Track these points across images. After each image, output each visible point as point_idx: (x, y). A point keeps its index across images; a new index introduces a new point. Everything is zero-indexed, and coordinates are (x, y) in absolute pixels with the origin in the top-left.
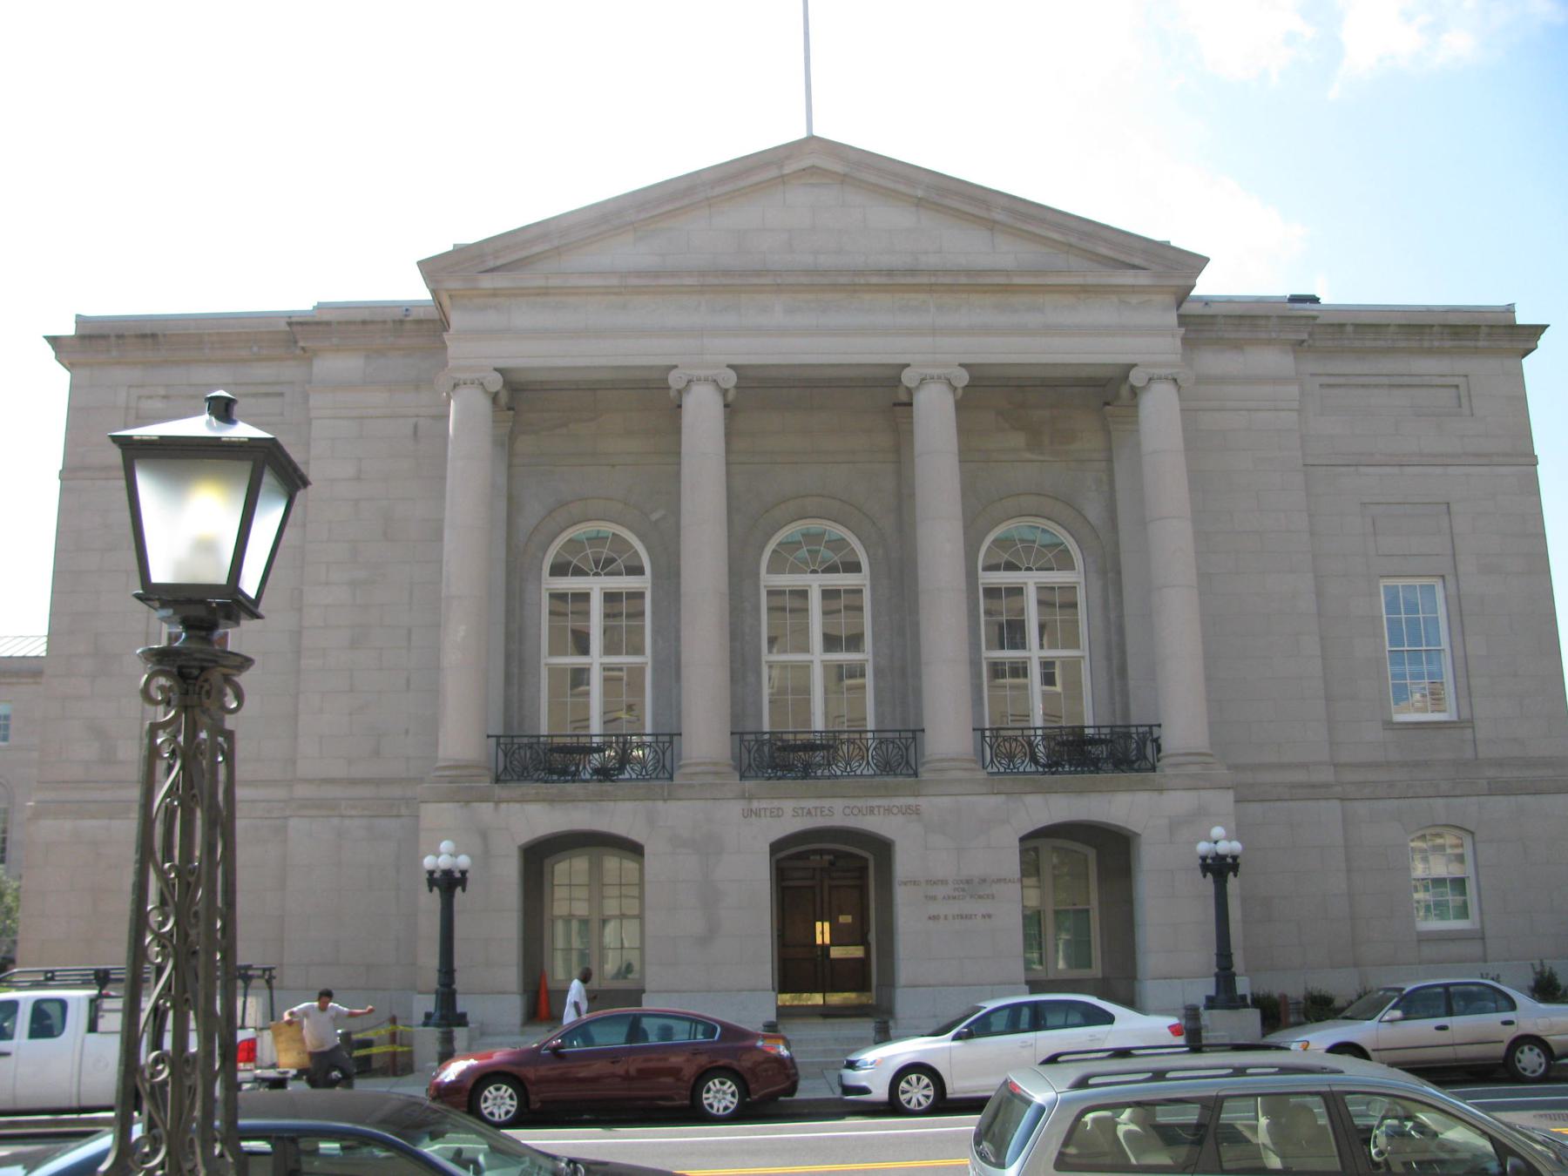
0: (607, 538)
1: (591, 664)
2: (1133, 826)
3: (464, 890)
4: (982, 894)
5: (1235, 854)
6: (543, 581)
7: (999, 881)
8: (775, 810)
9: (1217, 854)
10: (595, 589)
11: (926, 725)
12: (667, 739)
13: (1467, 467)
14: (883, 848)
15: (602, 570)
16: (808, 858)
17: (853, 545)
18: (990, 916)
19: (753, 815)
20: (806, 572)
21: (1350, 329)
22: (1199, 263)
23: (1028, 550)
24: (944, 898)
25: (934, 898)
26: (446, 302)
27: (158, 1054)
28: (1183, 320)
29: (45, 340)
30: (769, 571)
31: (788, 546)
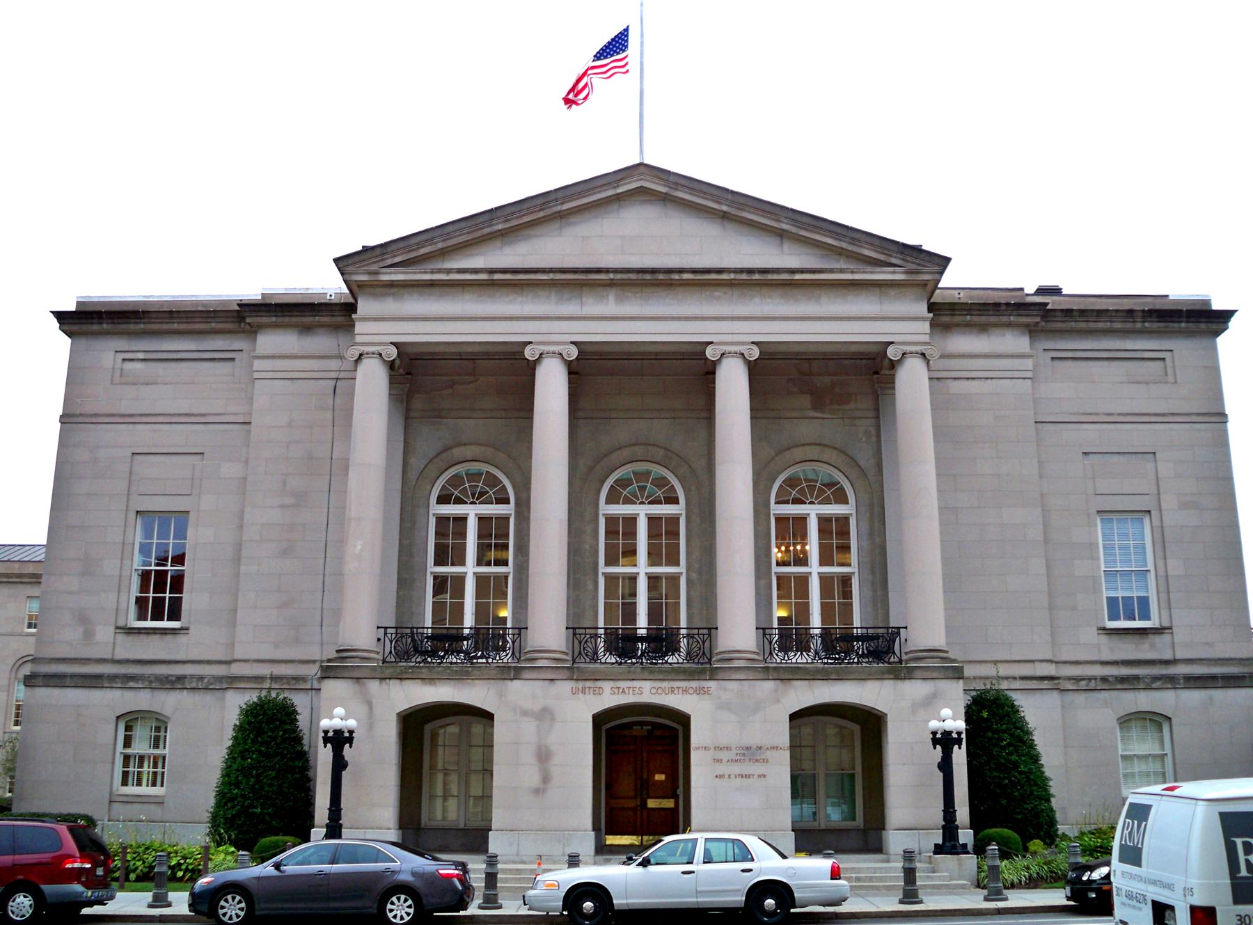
0: (483, 474)
1: (638, 573)
2: (880, 706)
3: (351, 747)
4: (759, 758)
5: (351, 729)
6: (431, 508)
7: (773, 748)
8: (597, 689)
9: (945, 731)
10: (470, 515)
11: (719, 625)
12: (705, 631)
13: (1153, 424)
14: (684, 720)
15: (646, 499)
16: (632, 728)
17: (673, 483)
18: (764, 776)
19: (580, 693)
20: (635, 503)
21: (1076, 314)
22: (945, 261)
23: (811, 488)
24: (728, 761)
25: (720, 761)
26: (355, 289)
27: (966, 884)
28: (932, 307)
29: (52, 315)
30: (607, 503)
31: (623, 483)
